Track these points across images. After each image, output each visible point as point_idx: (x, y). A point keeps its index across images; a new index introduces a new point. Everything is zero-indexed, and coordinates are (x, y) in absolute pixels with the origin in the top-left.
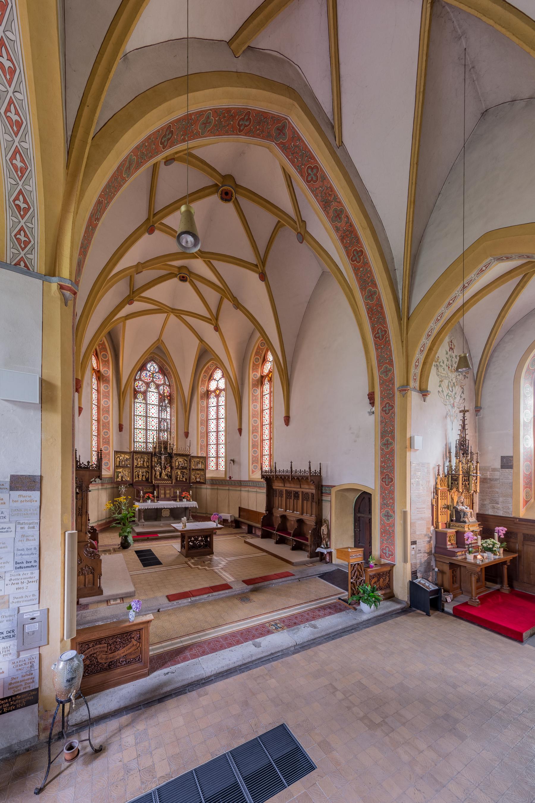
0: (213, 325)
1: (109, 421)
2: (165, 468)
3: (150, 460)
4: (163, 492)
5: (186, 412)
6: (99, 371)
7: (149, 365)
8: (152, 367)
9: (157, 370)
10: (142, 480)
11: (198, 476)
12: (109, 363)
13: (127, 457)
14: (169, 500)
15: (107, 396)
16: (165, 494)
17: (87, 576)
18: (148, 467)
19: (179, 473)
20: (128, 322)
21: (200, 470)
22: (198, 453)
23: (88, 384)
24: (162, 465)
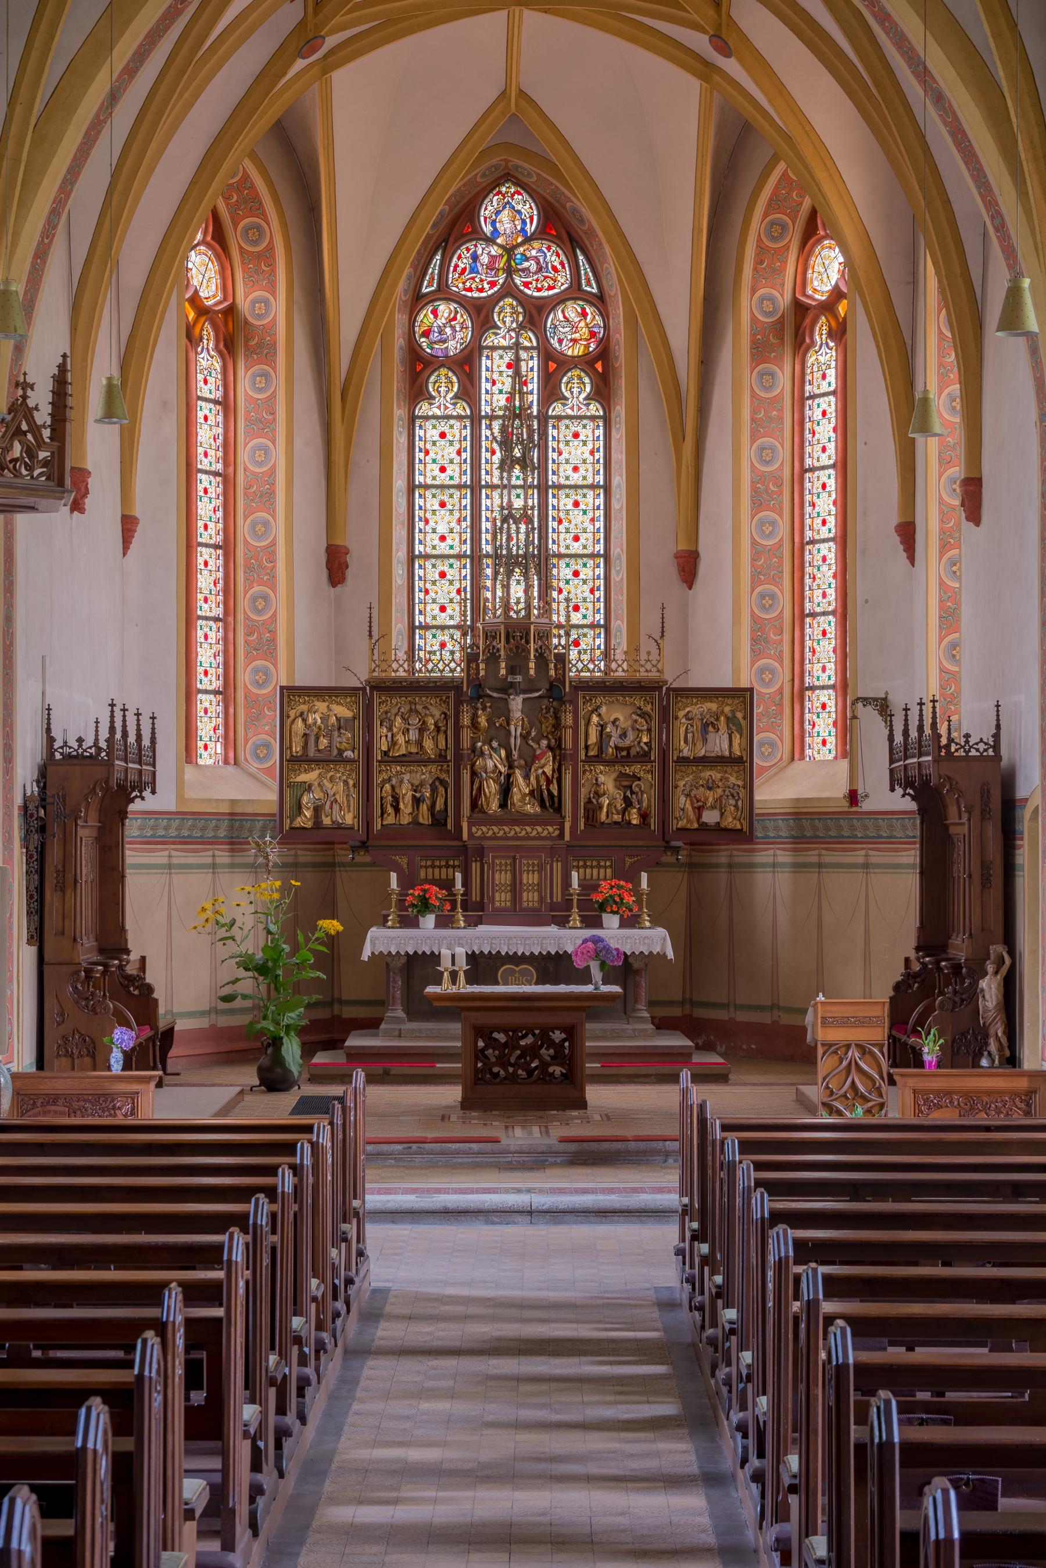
0: (704, 31)
1: (273, 544)
2: (530, 761)
3: (451, 722)
4: (502, 878)
5: (679, 437)
6: (231, 311)
7: (487, 211)
8: (505, 216)
9: (531, 229)
10: (415, 822)
11: (711, 797)
12: (272, 265)
13: (343, 711)
14: (534, 918)
15: (264, 427)
16: (515, 888)
17: (76, 1061)
18: (441, 757)
19: (607, 781)
20: (340, 77)
21: (718, 761)
22: (736, 670)
23: (165, 404)
24: (515, 741)
